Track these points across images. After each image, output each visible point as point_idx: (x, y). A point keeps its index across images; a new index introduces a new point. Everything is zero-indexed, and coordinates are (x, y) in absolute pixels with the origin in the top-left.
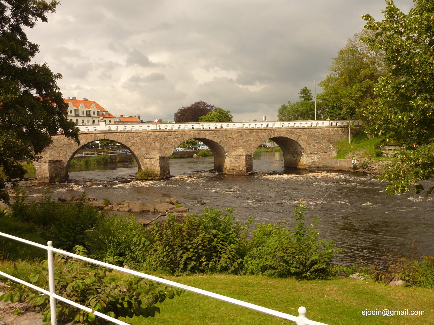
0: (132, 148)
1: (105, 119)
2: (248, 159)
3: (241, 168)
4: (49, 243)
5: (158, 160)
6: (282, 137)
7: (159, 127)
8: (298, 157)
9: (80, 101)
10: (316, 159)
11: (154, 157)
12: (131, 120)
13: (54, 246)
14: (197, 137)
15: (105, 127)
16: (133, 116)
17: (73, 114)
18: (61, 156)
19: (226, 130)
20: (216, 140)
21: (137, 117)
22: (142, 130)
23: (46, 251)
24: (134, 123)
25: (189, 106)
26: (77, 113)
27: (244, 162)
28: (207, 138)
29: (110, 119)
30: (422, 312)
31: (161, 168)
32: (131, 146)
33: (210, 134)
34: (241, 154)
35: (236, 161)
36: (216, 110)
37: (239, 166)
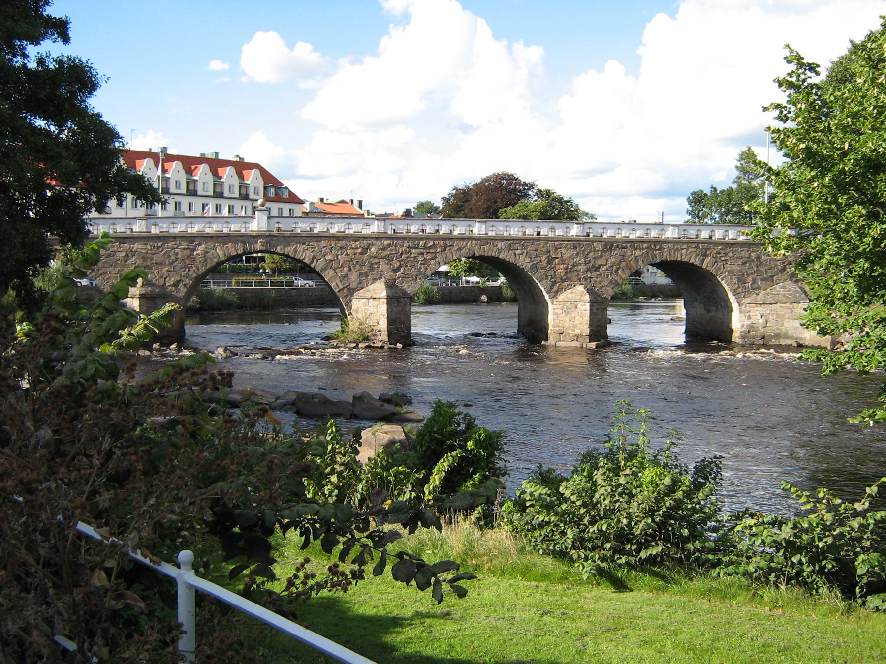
0: (328, 275)
1: (268, 204)
2: (597, 309)
3: (578, 332)
4: (185, 555)
5: (383, 302)
6: (681, 262)
7: (276, 225)
8: (717, 310)
9: (226, 163)
10: (759, 317)
11: (374, 296)
12: (342, 209)
13: (201, 568)
14: (477, 254)
15: (269, 224)
16: (348, 200)
17: (183, 190)
18: (167, 285)
19: (547, 240)
20: (523, 262)
21: (356, 203)
22: (299, 231)
23: (172, 582)
24: (331, 216)
25: (478, 181)
26: (191, 187)
27: (587, 318)
28: (501, 257)
29: (292, 206)
30: (82, 527)
31: (390, 321)
32: (325, 269)
33: (510, 248)
34: (577, 298)
35: (567, 313)
36: (540, 193)
37: (575, 326)
